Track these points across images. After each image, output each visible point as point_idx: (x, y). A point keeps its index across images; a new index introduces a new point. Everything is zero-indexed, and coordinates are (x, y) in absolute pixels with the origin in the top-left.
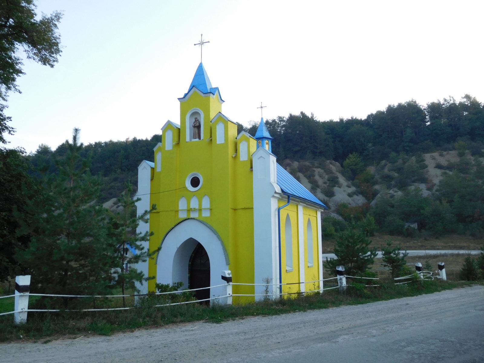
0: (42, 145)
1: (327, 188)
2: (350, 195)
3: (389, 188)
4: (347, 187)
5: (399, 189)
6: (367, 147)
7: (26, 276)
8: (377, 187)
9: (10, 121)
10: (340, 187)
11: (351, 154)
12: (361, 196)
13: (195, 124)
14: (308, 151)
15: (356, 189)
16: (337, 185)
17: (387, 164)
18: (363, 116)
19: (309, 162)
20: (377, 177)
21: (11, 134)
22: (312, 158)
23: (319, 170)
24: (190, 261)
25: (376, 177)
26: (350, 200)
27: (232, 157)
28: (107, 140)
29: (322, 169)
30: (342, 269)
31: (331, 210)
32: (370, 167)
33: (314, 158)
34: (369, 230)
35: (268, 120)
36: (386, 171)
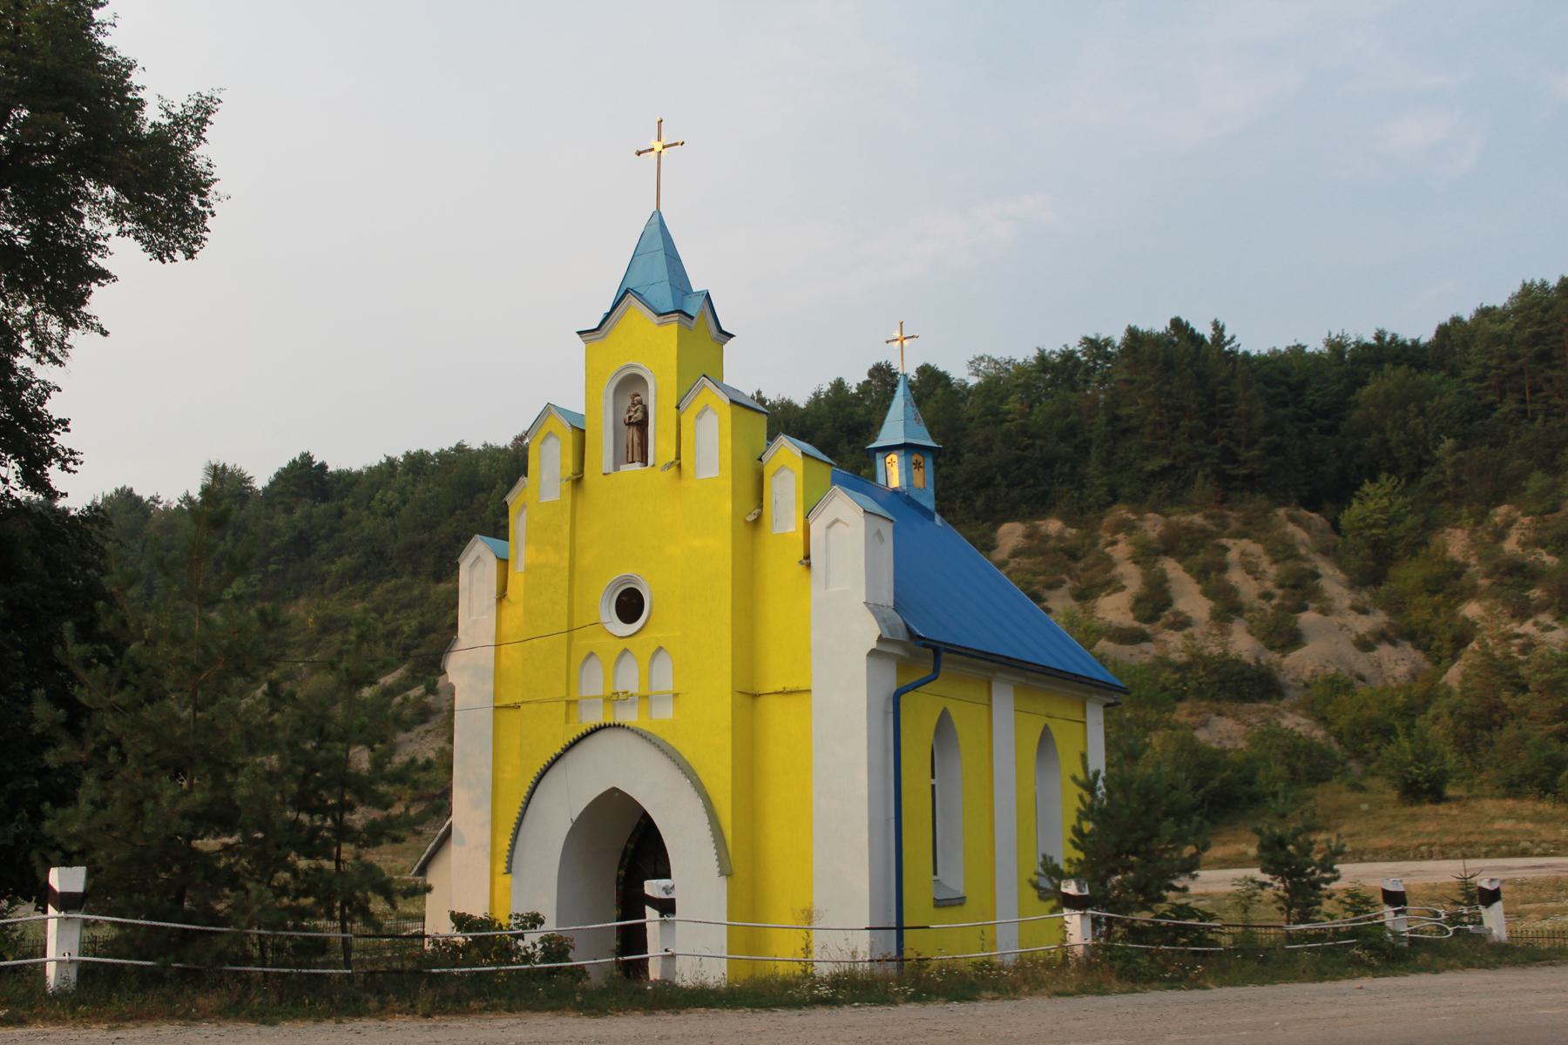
1: (1272, 615)
2: (1364, 645)
3: (1523, 612)
5: (1557, 619)
6: (1437, 454)
7: (75, 869)
8: (1472, 610)
9: (66, 433)
10: (1325, 611)
11: (1374, 480)
12: (1408, 646)
13: (631, 414)
14: (1200, 473)
15: (1386, 619)
16: (1312, 606)
17: (1515, 521)
19: (1207, 517)
20: (1475, 567)
21: (69, 471)
22: (1218, 499)
23: (1245, 544)
24: (620, 868)
25: (1470, 570)
26: (1361, 662)
27: (747, 522)
28: (448, 444)
29: (1255, 542)
30: (1080, 889)
31: (1283, 703)
32: (1448, 530)
33: (1223, 501)
34: (1420, 779)
36: (1511, 545)
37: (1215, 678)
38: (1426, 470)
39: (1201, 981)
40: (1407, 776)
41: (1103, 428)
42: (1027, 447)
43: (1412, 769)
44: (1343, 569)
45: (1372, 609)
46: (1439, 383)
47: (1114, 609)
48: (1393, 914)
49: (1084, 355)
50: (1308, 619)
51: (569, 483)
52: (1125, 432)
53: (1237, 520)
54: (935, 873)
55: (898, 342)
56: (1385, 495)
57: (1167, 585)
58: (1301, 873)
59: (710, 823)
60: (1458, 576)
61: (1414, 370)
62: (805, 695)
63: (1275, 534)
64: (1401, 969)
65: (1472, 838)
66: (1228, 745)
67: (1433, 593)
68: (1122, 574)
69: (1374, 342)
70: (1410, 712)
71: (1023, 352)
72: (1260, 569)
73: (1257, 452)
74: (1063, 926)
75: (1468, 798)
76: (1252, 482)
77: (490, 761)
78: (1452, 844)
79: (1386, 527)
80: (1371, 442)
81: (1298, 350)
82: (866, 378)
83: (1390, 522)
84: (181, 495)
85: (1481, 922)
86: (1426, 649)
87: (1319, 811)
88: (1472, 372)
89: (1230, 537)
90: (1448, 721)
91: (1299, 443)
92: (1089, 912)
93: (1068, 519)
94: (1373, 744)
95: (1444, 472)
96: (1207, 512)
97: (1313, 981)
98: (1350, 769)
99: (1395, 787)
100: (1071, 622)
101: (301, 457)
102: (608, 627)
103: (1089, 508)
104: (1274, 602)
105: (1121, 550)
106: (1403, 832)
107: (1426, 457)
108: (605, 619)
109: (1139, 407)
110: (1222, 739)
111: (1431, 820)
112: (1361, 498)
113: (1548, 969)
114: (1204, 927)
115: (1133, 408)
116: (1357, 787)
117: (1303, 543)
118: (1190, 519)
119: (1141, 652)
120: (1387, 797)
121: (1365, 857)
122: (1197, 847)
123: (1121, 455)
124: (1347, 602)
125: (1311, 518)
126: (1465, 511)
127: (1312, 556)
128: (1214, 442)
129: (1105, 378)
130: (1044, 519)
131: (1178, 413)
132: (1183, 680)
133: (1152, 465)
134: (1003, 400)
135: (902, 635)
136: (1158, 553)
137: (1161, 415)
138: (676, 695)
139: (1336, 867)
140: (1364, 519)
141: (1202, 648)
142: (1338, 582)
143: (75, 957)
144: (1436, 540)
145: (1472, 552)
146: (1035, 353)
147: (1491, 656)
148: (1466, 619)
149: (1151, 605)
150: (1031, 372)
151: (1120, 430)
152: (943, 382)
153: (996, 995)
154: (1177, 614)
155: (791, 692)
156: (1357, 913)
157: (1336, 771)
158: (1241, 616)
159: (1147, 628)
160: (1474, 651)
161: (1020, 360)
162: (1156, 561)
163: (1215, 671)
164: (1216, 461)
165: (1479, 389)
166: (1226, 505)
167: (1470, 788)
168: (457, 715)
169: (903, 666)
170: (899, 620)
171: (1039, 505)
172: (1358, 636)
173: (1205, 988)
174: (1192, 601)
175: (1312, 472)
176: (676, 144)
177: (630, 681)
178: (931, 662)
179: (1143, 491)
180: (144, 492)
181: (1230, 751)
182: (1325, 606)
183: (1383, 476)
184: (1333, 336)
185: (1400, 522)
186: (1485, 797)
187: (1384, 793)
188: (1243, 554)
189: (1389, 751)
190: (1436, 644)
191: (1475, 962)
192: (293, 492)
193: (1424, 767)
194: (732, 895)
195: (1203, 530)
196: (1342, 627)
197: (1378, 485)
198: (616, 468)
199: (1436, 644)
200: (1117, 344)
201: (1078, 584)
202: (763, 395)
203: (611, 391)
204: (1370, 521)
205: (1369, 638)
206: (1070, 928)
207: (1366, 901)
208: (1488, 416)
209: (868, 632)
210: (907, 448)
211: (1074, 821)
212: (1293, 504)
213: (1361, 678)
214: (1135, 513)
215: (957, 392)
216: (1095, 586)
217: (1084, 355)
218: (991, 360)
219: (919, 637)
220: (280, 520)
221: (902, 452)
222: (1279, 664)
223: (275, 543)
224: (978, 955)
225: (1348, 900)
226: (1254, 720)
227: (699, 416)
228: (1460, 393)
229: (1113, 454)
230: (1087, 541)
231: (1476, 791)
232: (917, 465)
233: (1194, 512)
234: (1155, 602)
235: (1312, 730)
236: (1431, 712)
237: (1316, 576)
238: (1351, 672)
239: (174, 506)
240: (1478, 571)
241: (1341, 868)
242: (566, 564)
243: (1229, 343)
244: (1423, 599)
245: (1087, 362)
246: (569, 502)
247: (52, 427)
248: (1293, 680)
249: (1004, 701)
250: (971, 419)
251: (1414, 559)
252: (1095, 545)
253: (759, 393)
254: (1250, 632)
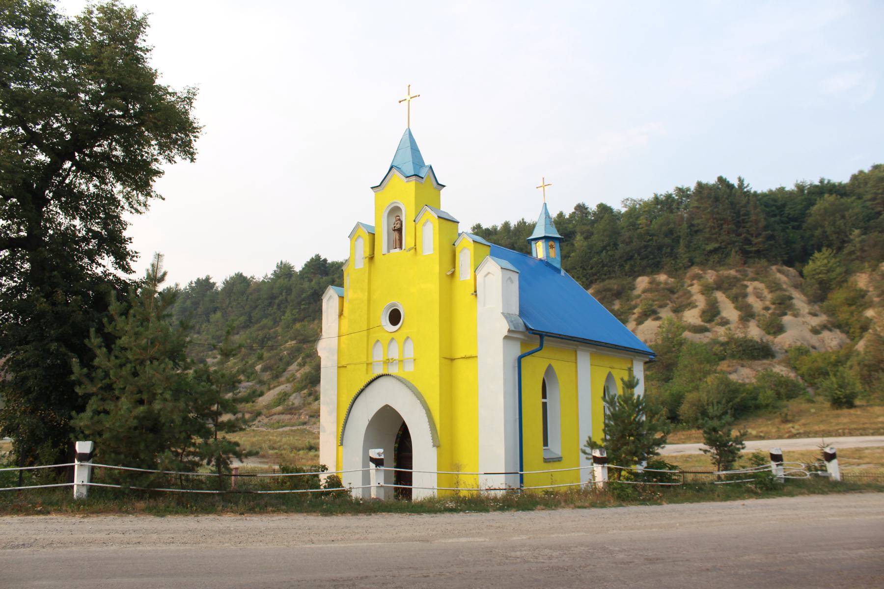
0: (281, 262)
1: (769, 318)
2: (815, 331)
4: (810, 316)
6: (851, 237)
10: (796, 315)
11: (820, 251)
12: (838, 331)
14: (733, 250)
16: (789, 313)
18: (841, 176)
19: (737, 271)
20: (872, 292)
21: (134, 261)
24: (396, 443)
25: (870, 294)
26: (814, 340)
27: (447, 275)
29: (761, 283)
30: (601, 454)
31: (775, 360)
32: (858, 274)
33: (745, 263)
34: (841, 396)
35: (658, 195)
37: (741, 348)
38: (846, 245)
39: (659, 501)
40: (835, 395)
41: (686, 230)
42: (649, 240)
43: (837, 392)
44: (805, 295)
45: (819, 314)
46: (852, 203)
47: (692, 317)
48: (775, 466)
49: (677, 196)
50: (787, 319)
51: (367, 259)
52: (696, 232)
53: (752, 272)
54: (546, 443)
55: (542, 188)
56: (825, 258)
57: (717, 305)
58: (725, 445)
59: (429, 421)
60: (863, 296)
61: (839, 197)
62: (475, 359)
63: (771, 279)
64: (774, 495)
65: (866, 426)
66: (747, 381)
67: (850, 305)
68: (696, 300)
69: (819, 184)
70: (838, 363)
71: (646, 195)
72: (763, 296)
73: (760, 239)
74: (592, 473)
75: (867, 406)
76: (759, 254)
77: (336, 392)
78: (855, 429)
79: (826, 273)
80: (817, 233)
81: (782, 190)
82: (574, 210)
83: (828, 271)
84: (264, 275)
85: (826, 471)
86: (847, 333)
87: (789, 413)
88: (869, 196)
89: (748, 280)
90: (857, 368)
91: (782, 234)
92: (606, 465)
93: (670, 274)
94: (819, 380)
95: (855, 246)
96: (737, 269)
97: (721, 501)
98: (808, 392)
99: (828, 400)
100: (671, 323)
101: (316, 256)
102: (385, 327)
103: (680, 268)
104: (770, 312)
105: (695, 288)
106: (831, 423)
107: (846, 239)
108: (384, 323)
109: (702, 220)
110: (744, 378)
111: (846, 416)
112: (813, 260)
113: (860, 495)
114: (671, 473)
115: (700, 220)
116: (810, 401)
117: (785, 283)
118: (728, 272)
119: (705, 337)
120: (825, 406)
121: (810, 435)
122: (664, 432)
123: (695, 243)
124: (807, 311)
125: (789, 271)
126: (866, 265)
127: (789, 289)
128: (740, 235)
129: (686, 206)
130: (658, 274)
131: (722, 222)
132: (725, 350)
133: (710, 247)
134: (638, 218)
135: (522, 328)
136: (713, 289)
137: (714, 223)
138: (414, 360)
139: (743, 442)
140: (815, 270)
141: (734, 334)
142: (803, 301)
143: (85, 483)
144: (852, 279)
145: (870, 285)
146: (653, 196)
147: (879, 336)
148: (867, 318)
149: (709, 314)
150: (651, 205)
151: (694, 231)
152: (610, 211)
153: (544, 507)
154: (722, 318)
155: (469, 358)
156: (759, 465)
157: (800, 393)
158: (754, 319)
159: (708, 325)
160: (870, 333)
161: (646, 199)
162: (712, 293)
163: (741, 345)
164: (741, 244)
165: (873, 204)
166: (747, 265)
167: (868, 401)
168: (322, 370)
169: (523, 343)
170: (521, 321)
171: (655, 267)
172: (812, 327)
173: (660, 504)
174: (730, 312)
175: (789, 248)
176: (416, 96)
177: (395, 353)
178: (538, 341)
179: (706, 260)
180: (247, 274)
181: (748, 384)
182: (796, 313)
183: (824, 249)
184: (799, 182)
185: (833, 271)
186: (875, 405)
187: (824, 403)
188: (755, 288)
189: (826, 383)
190: (852, 330)
191: (817, 491)
192: (312, 272)
193: (843, 390)
194: (439, 456)
195: (735, 278)
196: (804, 323)
197: (821, 253)
198: (389, 252)
199: (852, 330)
200: (692, 190)
201: (674, 305)
202: (525, 221)
203: (386, 215)
204: (818, 271)
205: (818, 328)
206: (596, 474)
207: (762, 459)
208: (877, 218)
209: (503, 327)
210: (546, 238)
211: (603, 420)
212: (779, 264)
213: (814, 347)
214: (702, 270)
215: (616, 216)
216: (683, 306)
217: (677, 196)
218: (632, 200)
219: (531, 329)
220: (306, 285)
221: (544, 240)
222: (773, 342)
223: (304, 295)
224: (548, 487)
225: (754, 459)
226: (760, 369)
227: (424, 225)
228: (863, 207)
229: (691, 242)
230: (679, 284)
231: (871, 402)
232: (552, 247)
233: (731, 269)
234: (712, 313)
235: (789, 373)
236: (849, 363)
237: (791, 298)
238: (809, 345)
239: (261, 280)
240: (873, 294)
241: (746, 443)
242: (366, 298)
243: (746, 187)
244: (845, 308)
245: (678, 199)
246: (367, 269)
247: (125, 241)
248: (780, 349)
249: (584, 360)
250: (623, 228)
251: (841, 289)
252: (682, 286)
253: (523, 219)
254: (758, 326)
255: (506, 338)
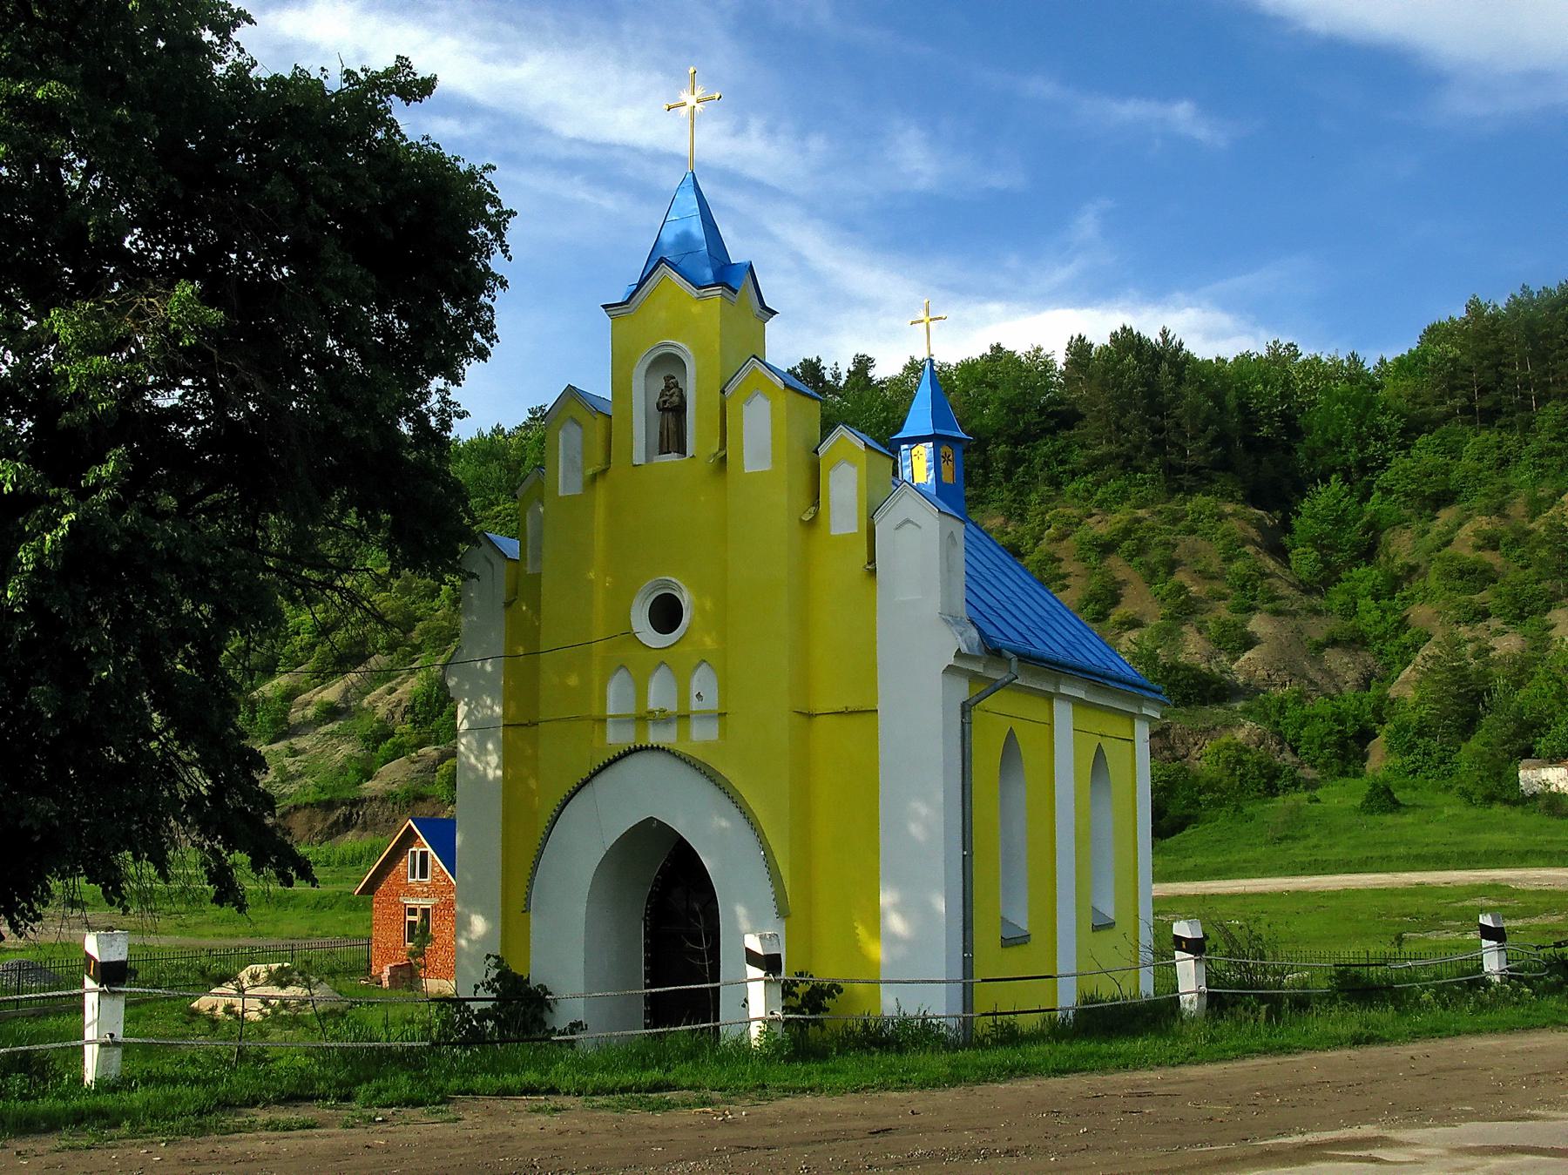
27: (801, 520)
177: (659, 695)
255: (950, 670)
